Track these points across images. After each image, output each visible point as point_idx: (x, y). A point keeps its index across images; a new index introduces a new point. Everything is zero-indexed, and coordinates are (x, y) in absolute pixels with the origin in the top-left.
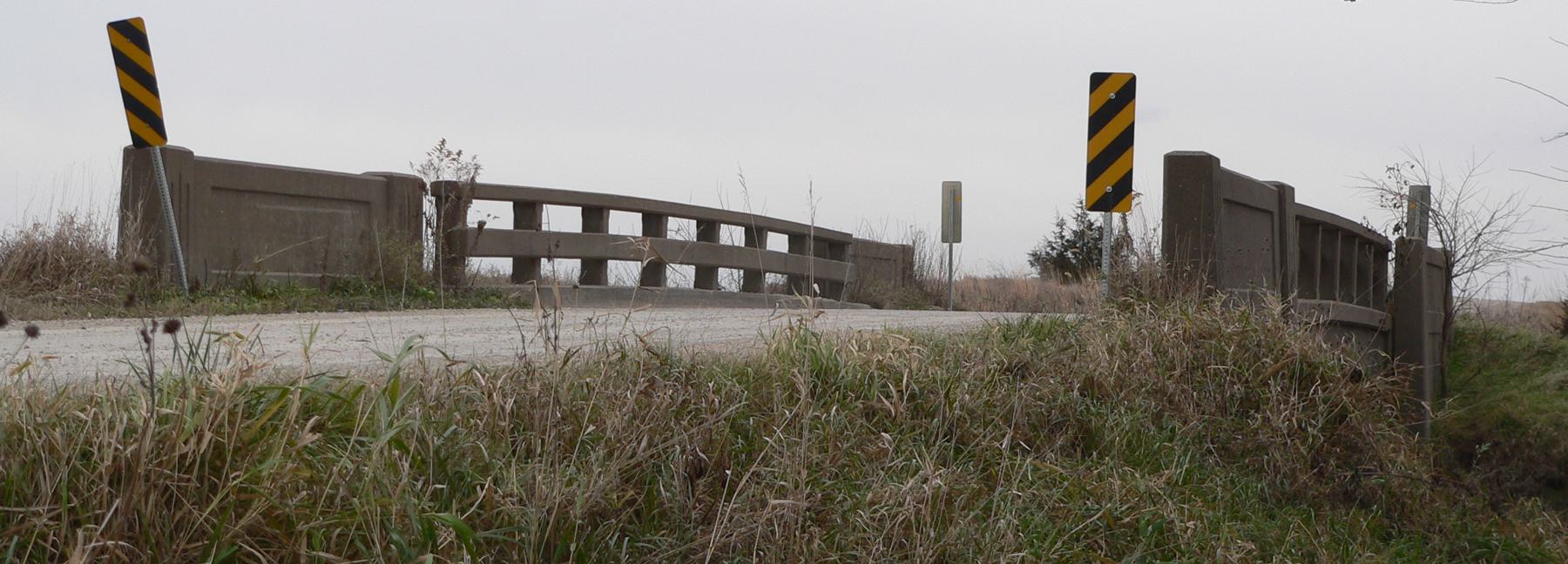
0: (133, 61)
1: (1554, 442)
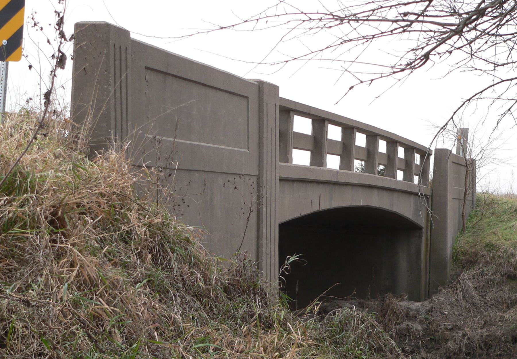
1: (513, 255)
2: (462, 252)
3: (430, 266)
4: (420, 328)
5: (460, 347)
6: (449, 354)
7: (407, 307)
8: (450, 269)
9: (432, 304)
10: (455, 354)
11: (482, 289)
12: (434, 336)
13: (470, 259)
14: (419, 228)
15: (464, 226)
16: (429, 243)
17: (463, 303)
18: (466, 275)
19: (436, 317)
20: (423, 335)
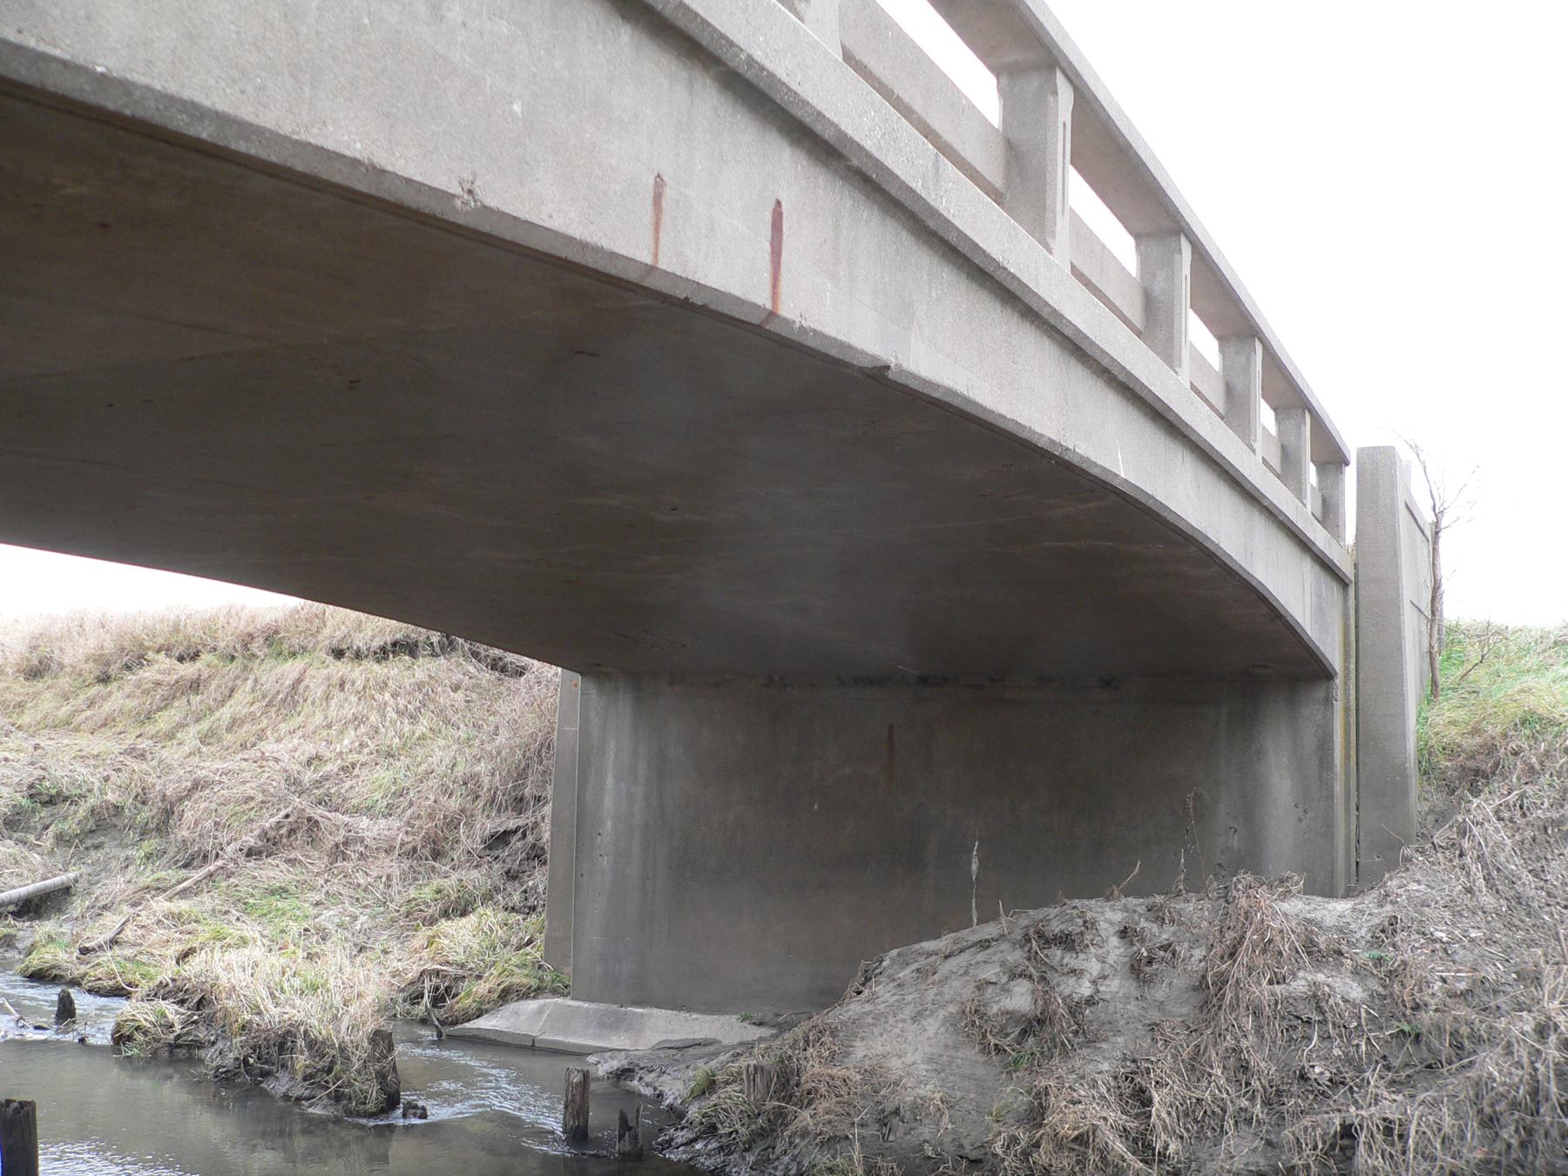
0: (734, 296)
2: (1444, 749)
3: (1358, 790)
4: (1357, 992)
5: (1534, 1077)
6: (1492, 1105)
7: (1306, 919)
8: (1420, 799)
9: (1389, 907)
10: (1515, 1105)
11: (1531, 851)
12: (1409, 1023)
13: (1471, 764)
14: (1323, 673)
15: (1434, 683)
16: (1353, 720)
17: (1488, 900)
18: (1482, 806)
19: (1409, 950)
20: (1372, 1019)
